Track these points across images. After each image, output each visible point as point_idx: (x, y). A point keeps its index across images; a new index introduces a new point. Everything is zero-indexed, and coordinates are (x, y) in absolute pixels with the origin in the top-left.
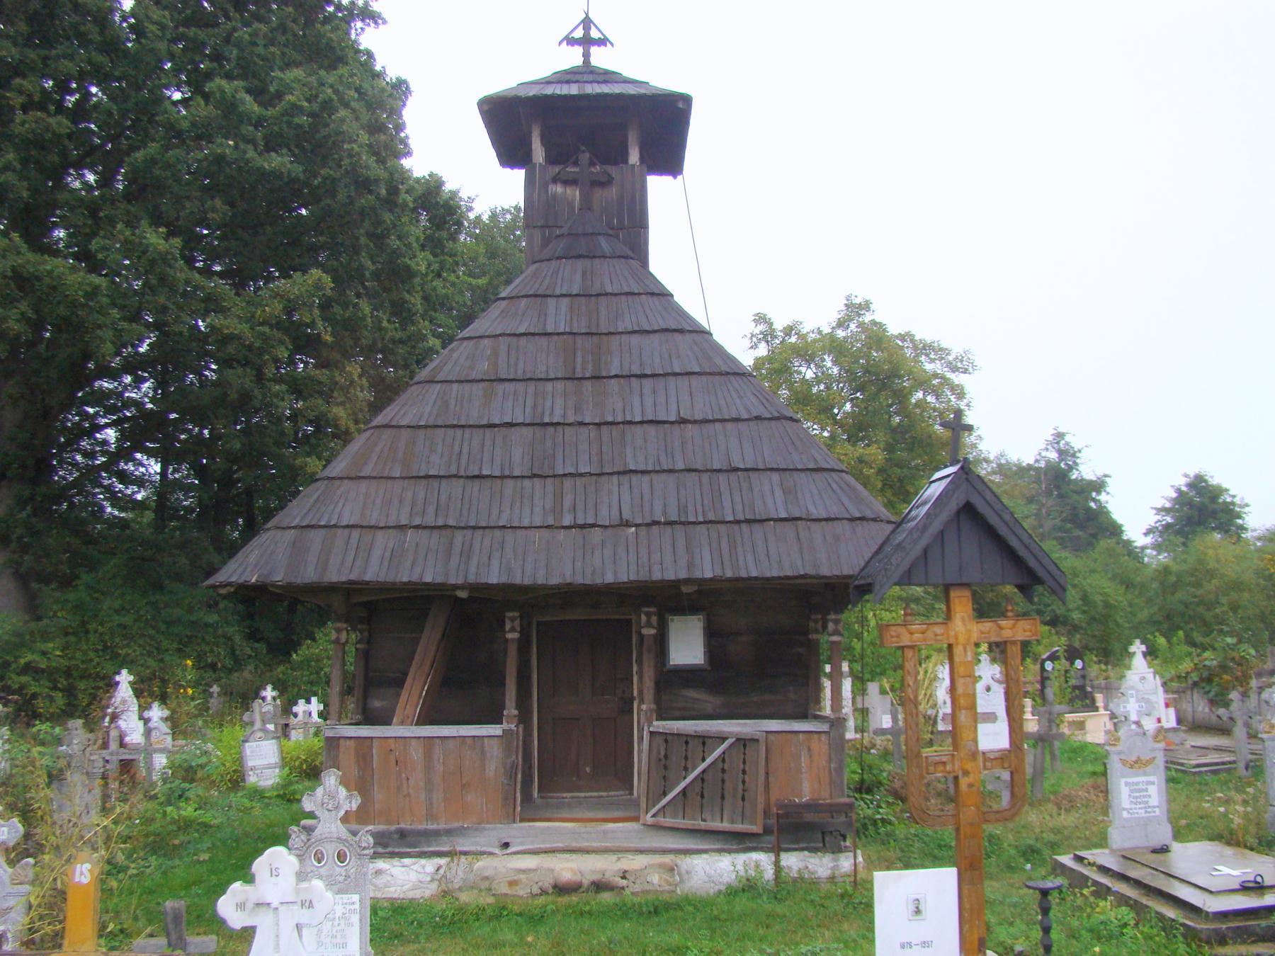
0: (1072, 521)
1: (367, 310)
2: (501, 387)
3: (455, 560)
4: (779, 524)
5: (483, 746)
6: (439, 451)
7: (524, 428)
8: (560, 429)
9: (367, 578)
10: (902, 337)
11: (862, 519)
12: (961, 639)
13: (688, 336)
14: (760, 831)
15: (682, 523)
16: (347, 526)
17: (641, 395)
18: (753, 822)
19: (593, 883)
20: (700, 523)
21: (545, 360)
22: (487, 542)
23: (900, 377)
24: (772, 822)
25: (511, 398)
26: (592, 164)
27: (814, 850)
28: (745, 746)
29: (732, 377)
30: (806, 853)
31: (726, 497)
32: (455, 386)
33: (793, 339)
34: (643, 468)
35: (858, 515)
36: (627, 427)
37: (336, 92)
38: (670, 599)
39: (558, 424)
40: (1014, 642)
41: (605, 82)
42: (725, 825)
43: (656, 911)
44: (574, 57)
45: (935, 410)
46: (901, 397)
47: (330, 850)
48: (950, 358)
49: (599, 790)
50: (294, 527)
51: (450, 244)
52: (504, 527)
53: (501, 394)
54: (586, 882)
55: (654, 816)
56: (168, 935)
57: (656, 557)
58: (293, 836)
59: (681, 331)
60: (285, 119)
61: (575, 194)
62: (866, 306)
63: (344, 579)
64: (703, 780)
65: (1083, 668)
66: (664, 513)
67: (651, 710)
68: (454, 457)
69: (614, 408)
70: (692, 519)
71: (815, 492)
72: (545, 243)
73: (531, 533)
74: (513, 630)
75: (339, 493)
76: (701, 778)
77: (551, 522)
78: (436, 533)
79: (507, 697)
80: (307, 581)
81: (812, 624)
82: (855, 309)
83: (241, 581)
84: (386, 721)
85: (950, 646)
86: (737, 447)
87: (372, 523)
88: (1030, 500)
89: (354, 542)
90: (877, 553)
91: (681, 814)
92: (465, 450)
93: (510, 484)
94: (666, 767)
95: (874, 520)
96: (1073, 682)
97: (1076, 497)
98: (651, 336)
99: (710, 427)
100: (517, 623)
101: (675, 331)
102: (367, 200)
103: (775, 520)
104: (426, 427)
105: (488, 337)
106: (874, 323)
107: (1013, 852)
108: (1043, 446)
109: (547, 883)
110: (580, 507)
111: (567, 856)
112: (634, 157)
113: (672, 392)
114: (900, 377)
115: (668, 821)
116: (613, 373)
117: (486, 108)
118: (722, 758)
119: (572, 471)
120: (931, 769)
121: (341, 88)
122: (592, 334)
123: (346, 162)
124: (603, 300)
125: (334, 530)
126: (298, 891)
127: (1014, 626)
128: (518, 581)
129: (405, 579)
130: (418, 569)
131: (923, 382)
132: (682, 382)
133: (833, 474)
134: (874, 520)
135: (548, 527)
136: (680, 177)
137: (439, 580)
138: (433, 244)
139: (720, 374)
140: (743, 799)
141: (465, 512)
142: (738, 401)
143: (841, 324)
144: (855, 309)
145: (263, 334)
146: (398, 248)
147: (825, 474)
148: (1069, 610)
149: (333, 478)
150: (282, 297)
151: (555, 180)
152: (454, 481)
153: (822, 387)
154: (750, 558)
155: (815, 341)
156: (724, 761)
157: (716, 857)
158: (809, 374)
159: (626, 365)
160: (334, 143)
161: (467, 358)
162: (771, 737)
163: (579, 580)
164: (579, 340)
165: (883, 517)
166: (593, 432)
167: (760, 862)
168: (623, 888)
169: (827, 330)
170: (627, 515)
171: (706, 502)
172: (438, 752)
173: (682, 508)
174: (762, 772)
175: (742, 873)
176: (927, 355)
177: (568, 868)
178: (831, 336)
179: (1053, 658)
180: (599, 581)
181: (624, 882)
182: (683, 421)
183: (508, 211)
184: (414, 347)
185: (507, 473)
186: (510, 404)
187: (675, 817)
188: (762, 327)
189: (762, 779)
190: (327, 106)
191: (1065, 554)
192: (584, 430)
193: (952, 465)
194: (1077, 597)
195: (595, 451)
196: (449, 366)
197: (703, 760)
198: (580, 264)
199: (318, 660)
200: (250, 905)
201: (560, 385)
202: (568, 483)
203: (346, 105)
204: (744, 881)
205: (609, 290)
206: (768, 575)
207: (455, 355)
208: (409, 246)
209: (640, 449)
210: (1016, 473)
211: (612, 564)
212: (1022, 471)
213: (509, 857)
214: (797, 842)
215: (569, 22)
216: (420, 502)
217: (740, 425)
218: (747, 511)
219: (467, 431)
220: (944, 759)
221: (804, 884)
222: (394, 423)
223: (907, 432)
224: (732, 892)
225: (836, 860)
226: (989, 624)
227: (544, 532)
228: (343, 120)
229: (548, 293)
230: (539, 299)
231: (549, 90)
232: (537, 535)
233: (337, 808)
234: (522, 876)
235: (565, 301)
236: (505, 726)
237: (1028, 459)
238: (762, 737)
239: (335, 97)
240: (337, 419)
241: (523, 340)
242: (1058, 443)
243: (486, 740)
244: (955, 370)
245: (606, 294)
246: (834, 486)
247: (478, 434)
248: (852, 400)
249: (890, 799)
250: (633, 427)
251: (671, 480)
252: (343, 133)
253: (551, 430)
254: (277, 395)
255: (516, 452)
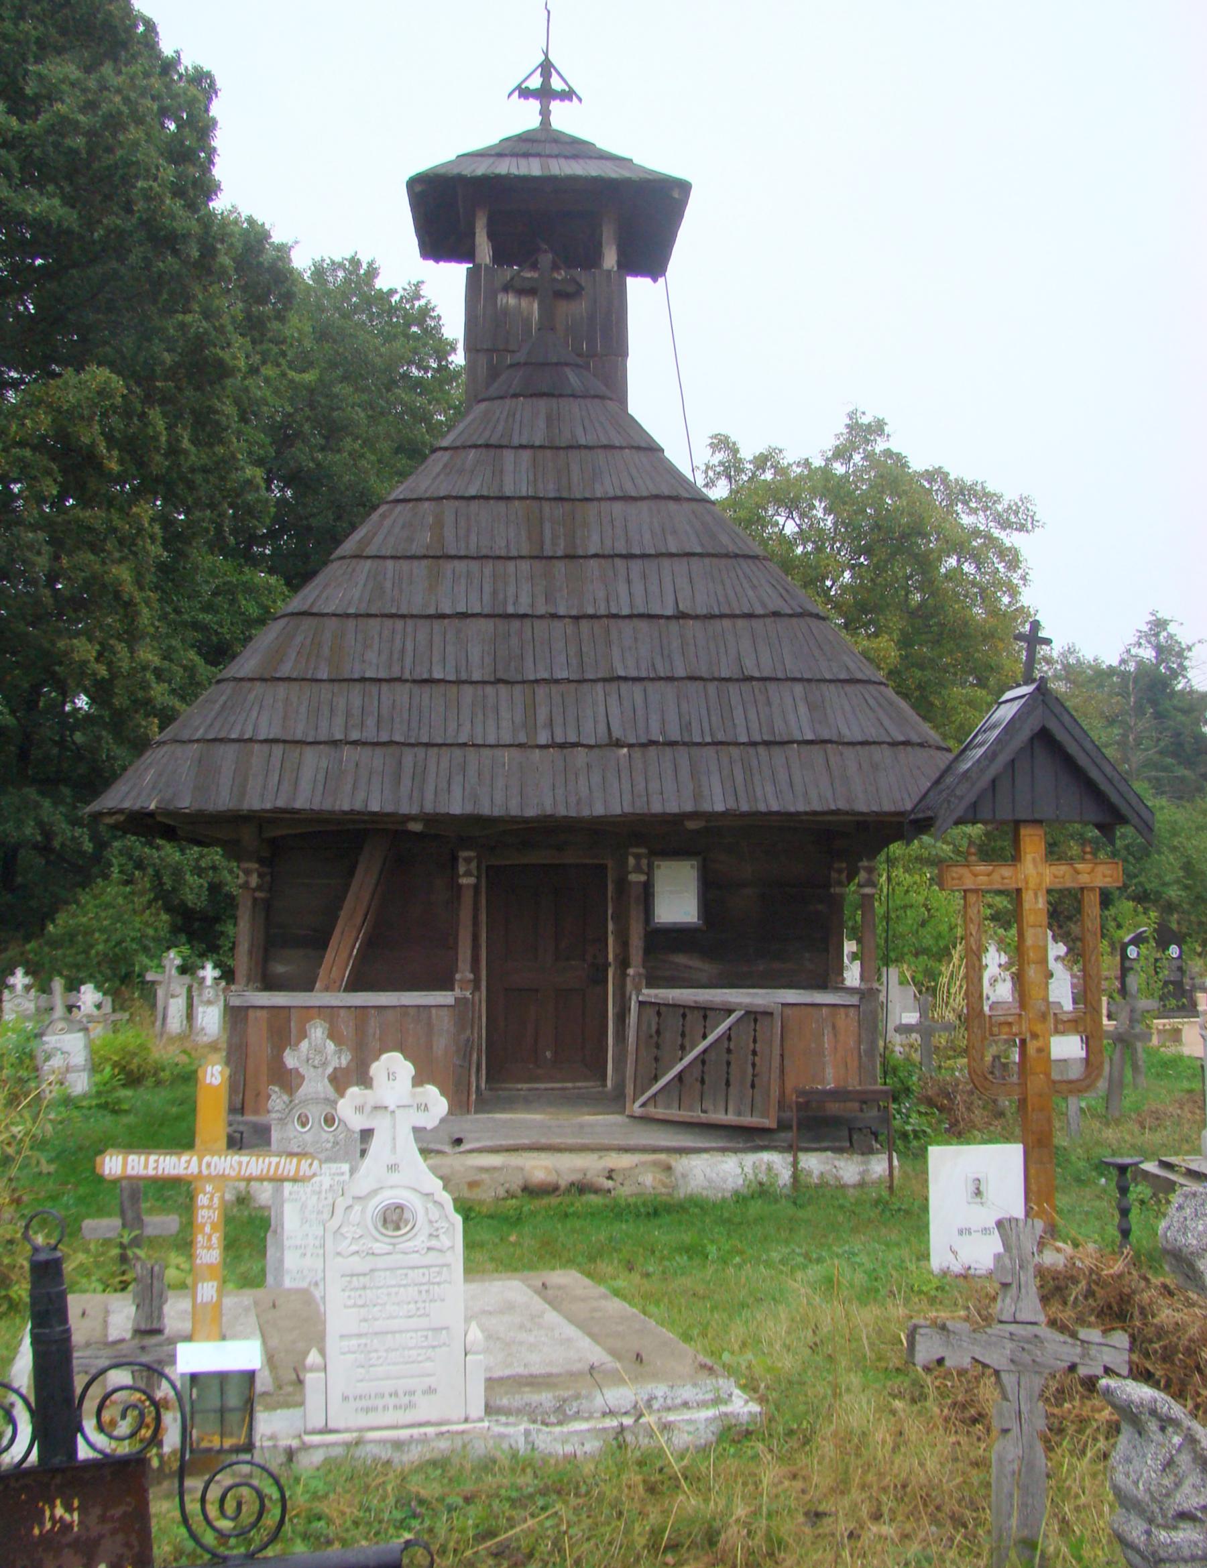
0: (1174, 755)
1: (161, 425)
2: (448, 566)
3: (406, 782)
4: (805, 749)
5: (430, 1017)
6: (376, 647)
7: (482, 621)
8: (528, 622)
9: (298, 805)
10: (930, 476)
11: (906, 743)
12: (1032, 884)
13: (686, 505)
14: (774, 1125)
15: (685, 744)
16: (266, 741)
17: (629, 582)
18: (765, 1114)
19: (572, 1184)
20: (708, 744)
21: (503, 531)
22: (444, 764)
23: (925, 535)
24: (791, 1115)
25: (463, 581)
26: (555, 267)
27: (839, 1150)
28: (756, 1020)
29: (741, 560)
30: (829, 1154)
31: (738, 712)
32: (390, 564)
33: (768, 476)
34: (634, 674)
35: (901, 738)
36: (612, 621)
37: (127, 100)
38: (665, 836)
39: (525, 616)
40: (1092, 889)
41: (575, 157)
42: (731, 1118)
43: (656, 1213)
44: (527, 117)
45: (974, 584)
46: (926, 564)
47: (315, 1113)
48: (1000, 508)
49: (564, 1080)
50: (198, 741)
51: (276, 325)
52: (465, 745)
53: (449, 574)
54: (563, 1183)
55: (643, 1105)
56: (123, 1214)
57: (654, 786)
58: (274, 1097)
59: (676, 499)
60: (51, 139)
61: (532, 308)
62: (878, 428)
63: (268, 806)
64: (703, 1062)
65: (1180, 957)
66: (663, 732)
67: (640, 975)
68: (396, 656)
69: (595, 600)
70: (697, 739)
71: (847, 708)
72: (494, 373)
73: (498, 752)
74: (468, 874)
75: (251, 697)
76: (702, 1059)
77: (522, 739)
78: (379, 751)
79: (460, 957)
80: (222, 808)
81: (834, 875)
82: (862, 432)
83: (137, 807)
84: (309, 987)
85: (1019, 891)
86: (749, 651)
87: (299, 737)
88: (1111, 721)
89: (276, 761)
90: (937, 782)
91: (676, 1105)
92: (409, 647)
93: (468, 690)
94: (658, 1046)
95: (921, 745)
96: (1165, 974)
97: (1181, 717)
98: (639, 504)
99: (717, 622)
100: (474, 865)
101: (670, 498)
102: (168, 264)
103: (799, 743)
104: (357, 616)
105: (428, 499)
106: (888, 453)
107: (1081, 1164)
108: (1134, 640)
109: (516, 1184)
110: (558, 720)
111: (535, 1154)
112: (610, 259)
113: (667, 580)
114: (925, 535)
115: (660, 1112)
116: (592, 551)
117: (418, 188)
118: (728, 1036)
119: (546, 675)
120: (995, 1030)
121: (133, 95)
122: (561, 499)
123: (140, 206)
124: (574, 455)
125: (250, 745)
126: (414, 1095)
127: (1092, 870)
128: (486, 810)
129: (346, 807)
130: (361, 796)
131: (959, 545)
132: (681, 566)
133: (871, 688)
134: (921, 745)
135: (520, 745)
136: (661, 280)
137: (389, 809)
138: (253, 326)
139: (727, 556)
140: (753, 1086)
141: (414, 725)
142: (750, 593)
143: (841, 453)
144: (862, 432)
145: (21, 459)
146: (206, 333)
147: (859, 687)
148: (1165, 884)
149: (242, 679)
150: (50, 405)
151: (506, 289)
152: (397, 685)
153: (810, 547)
154: (769, 789)
155: (800, 477)
156: (729, 1039)
157: (717, 1157)
158: (790, 528)
159: (608, 542)
160: (123, 178)
161: (403, 527)
162: (788, 1011)
163: (562, 811)
164: (546, 506)
165: (931, 742)
166: (569, 626)
167: (775, 1164)
168: (609, 1191)
169: (818, 462)
170: (617, 733)
171: (714, 718)
172: (373, 1025)
173: (686, 727)
174: (776, 1051)
175: (751, 1176)
176: (965, 503)
177: (539, 1167)
178: (826, 471)
179: (1138, 940)
180: (586, 813)
181: (609, 1184)
182: (681, 616)
183: (341, 266)
184: (223, 479)
185: (464, 676)
186: (463, 588)
187: (668, 1107)
188: (720, 456)
189: (776, 1063)
190: (114, 123)
191: (1163, 801)
192: (557, 624)
193: (1026, 683)
194: (1177, 865)
195: (573, 650)
196: (378, 539)
197: (704, 1037)
198: (542, 404)
199: (86, 934)
200: (368, 1108)
201: (525, 566)
202: (541, 691)
203: (139, 121)
204: (754, 1185)
205: (582, 442)
206: (792, 809)
207: (387, 523)
208: (221, 330)
209: (631, 651)
210: (1091, 680)
211: (603, 793)
212: (1102, 675)
213: (463, 1157)
214: (817, 1139)
215: (524, 69)
216: (356, 712)
217: (754, 622)
218: (764, 729)
219: (410, 622)
220: (1010, 1019)
221: (829, 1190)
222: (315, 610)
223: (932, 616)
224: (740, 1199)
225: (867, 1163)
226: (1063, 868)
227: (514, 752)
228: (136, 144)
229: (504, 443)
230: (492, 452)
231: (504, 167)
232: (506, 755)
233: (325, 1064)
234: (485, 1176)
235: (526, 455)
236: (458, 992)
237: (1110, 659)
238: (777, 1010)
239: (125, 110)
240: (119, 582)
241: (474, 505)
242: (1157, 635)
243: (434, 1011)
244: (1005, 525)
245: (579, 447)
246: (871, 701)
247: (424, 625)
248: (852, 567)
249: (922, 1109)
250: (620, 621)
251: (669, 690)
252: (138, 163)
253: (516, 624)
254: (30, 547)
255: (474, 650)
